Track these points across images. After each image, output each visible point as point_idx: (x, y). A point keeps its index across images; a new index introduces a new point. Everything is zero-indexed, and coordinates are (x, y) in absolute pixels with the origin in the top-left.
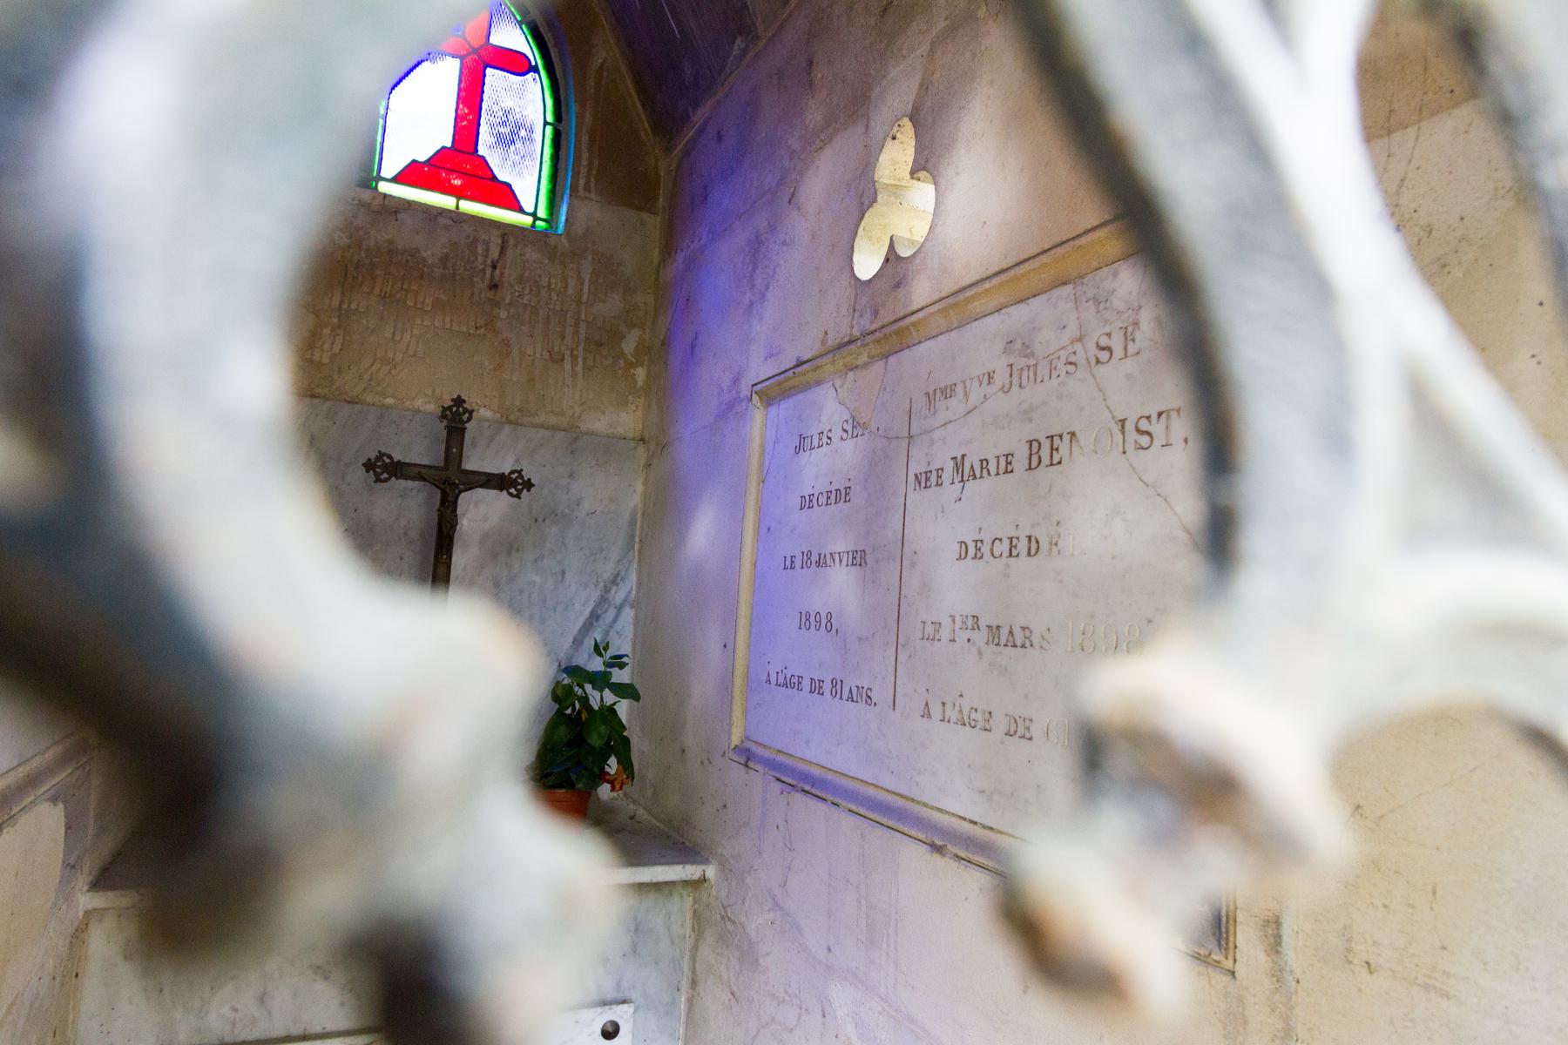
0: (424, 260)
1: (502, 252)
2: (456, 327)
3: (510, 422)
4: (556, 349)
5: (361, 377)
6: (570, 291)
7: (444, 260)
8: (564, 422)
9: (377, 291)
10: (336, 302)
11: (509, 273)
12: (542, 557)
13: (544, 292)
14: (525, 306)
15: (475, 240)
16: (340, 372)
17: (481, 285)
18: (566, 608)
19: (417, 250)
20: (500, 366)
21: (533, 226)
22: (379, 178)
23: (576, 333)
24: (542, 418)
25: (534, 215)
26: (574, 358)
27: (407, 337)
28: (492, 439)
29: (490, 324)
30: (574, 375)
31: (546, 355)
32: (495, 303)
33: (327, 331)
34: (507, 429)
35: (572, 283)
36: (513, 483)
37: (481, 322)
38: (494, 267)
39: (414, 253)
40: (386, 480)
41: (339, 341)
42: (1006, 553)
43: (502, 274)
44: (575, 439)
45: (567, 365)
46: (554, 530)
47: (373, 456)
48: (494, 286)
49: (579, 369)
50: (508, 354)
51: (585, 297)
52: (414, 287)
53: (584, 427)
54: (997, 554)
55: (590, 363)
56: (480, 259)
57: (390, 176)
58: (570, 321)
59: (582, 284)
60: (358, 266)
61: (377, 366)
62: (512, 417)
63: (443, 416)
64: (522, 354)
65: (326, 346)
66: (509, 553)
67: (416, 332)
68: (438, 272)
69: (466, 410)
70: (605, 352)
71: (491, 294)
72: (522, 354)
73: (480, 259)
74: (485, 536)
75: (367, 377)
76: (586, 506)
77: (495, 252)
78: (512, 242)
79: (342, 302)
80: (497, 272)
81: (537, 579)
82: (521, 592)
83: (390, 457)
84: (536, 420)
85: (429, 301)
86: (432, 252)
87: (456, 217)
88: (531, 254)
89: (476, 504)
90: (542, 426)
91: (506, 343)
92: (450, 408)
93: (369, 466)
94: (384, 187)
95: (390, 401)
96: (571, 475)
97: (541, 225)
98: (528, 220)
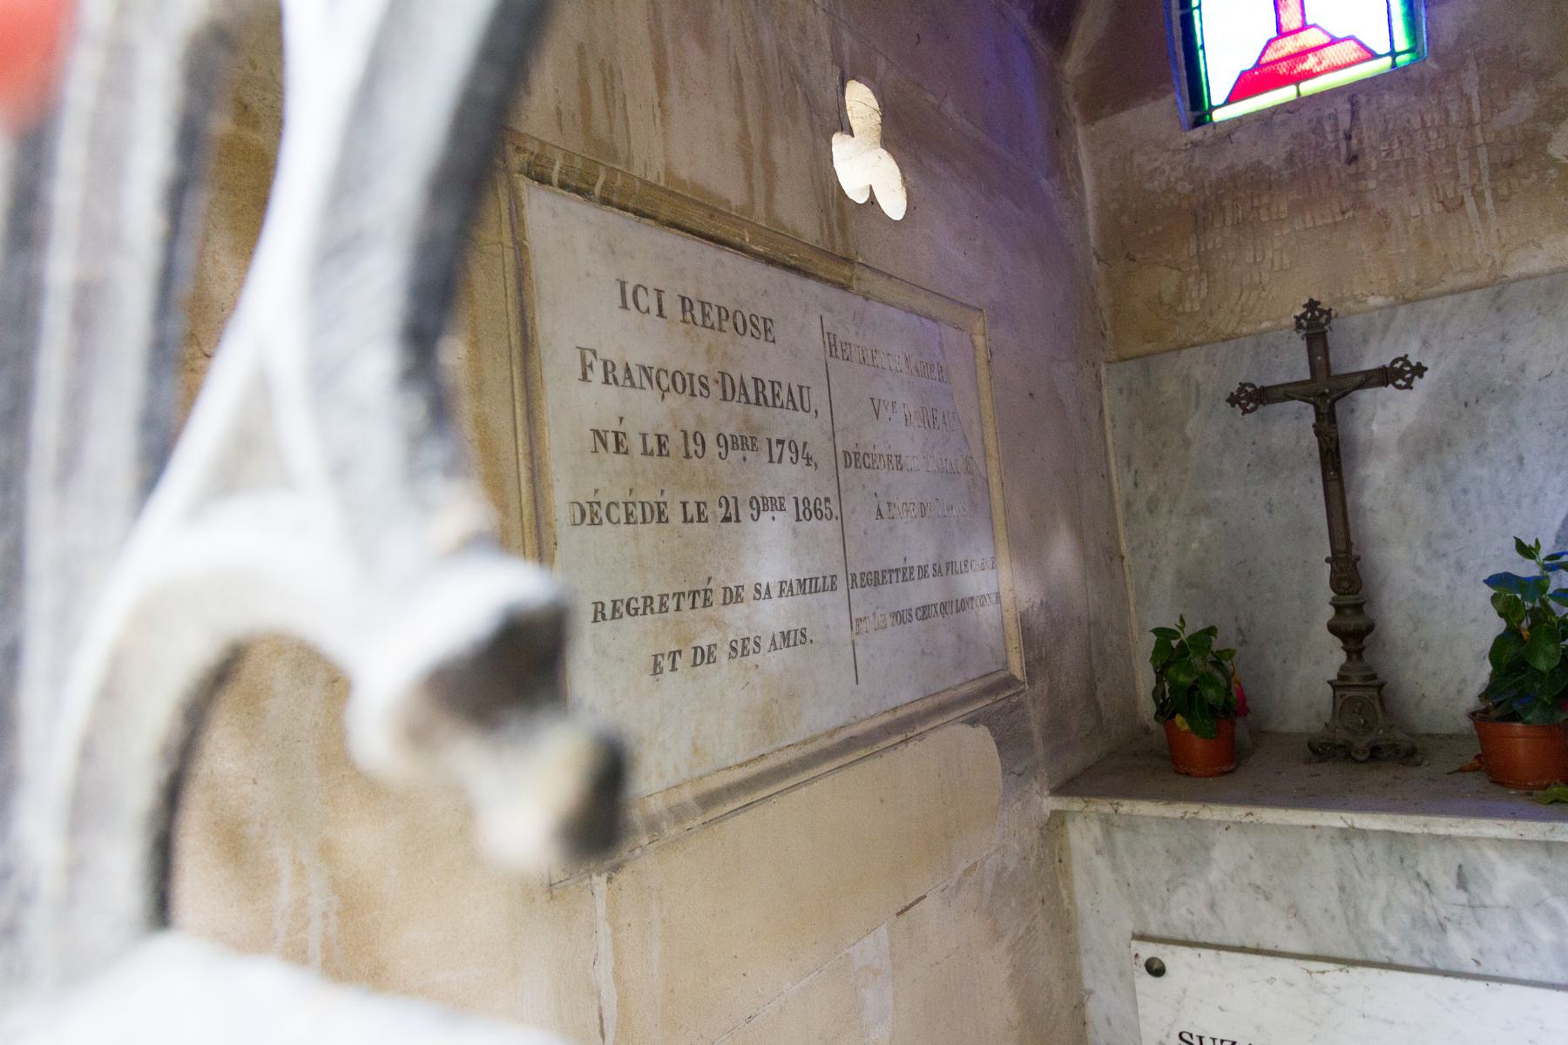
0: (1269, 168)
1: (1354, 114)
2: (1319, 222)
3: (1407, 301)
4: (1450, 194)
5: (1232, 312)
6: (1454, 118)
7: (1290, 158)
8: (1482, 276)
9: (1229, 222)
10: (1193, 250)
11: (1369, 135)
12: (1484, 446)
13: (1418, 138)
14: (1397, 164)
15: (1319, 120)
16: (1211, 313)
17: (1336, 164)
18: (1535, 501)
19: (1259, 162)
20: (1381, 244)
21: (1394, 65)
22: (1212, 108)
23: (1475, 164)
24: (1450, 281)
25: (1393, 54)
26: (1479, 197)
27: (1269, 254)
28: (1386, 328)
29: (1359, 202)
30: (1483, 215)
31: (1438, 207)
32: (1359, 176)
33: (1191, 280)
34: (1403, 311)
35: (1453, 108)
36: (1400, 373)
37: (1346, 204)
38: (1348, 138)
39: (1257, 166)
40: (1252, 410)
41: (1204, 285)
42: (623, 520)
43: (1360, 142)
44: (1499, 294)
45: (1470, 206)
46: (1494, 411)
47: (1234, 389)
48: (1353, 159)
49: (1489, 205)
50: (1388, 227)
51: (1477, 117)
52: (1265, 200)
53: (1511, 273)
54: (614, 519)
55: (1504, 191)
56: (1330, 137)
57: (1222, 101)
58: (1461, 153)
59: (1469, 101)
60: (1205, 207)
61: (1246, 293)
62: (1409, 295)
63: (1299, 326)
64: (1406, 220)
65: (1194, 294)
66: (1439, 449)
67: (1277, 244)
68: (1286, 174)
69: (1322, 312)
70: (1521, 169)
71: (1352, 169)
72: (1406, 220)
73: (1330, 137)
74: (1402, 441)
75: (1238, 309)
76: (1535, 370)
77: (1345, 121)
78: (1362, 99)
79: (1199, 246)
80: (1354, 141)
81: (1484, 472)
82: (1465, 491)
83: (1252, 385)
84: (1445, 287)
85: (1283, 208)
86: (1273, 154)
87: (1300, 103)
88: (1391, 101)
89: (1384, 405)
90: (1452, 292)
91: (1383, 214)
92: (1303, 316)
93: (1233, 400)
94: (1217, 116)
95: (1266, 325)
96: (1504, 338)
97: (1402, 60)
98: (1383, 65)
